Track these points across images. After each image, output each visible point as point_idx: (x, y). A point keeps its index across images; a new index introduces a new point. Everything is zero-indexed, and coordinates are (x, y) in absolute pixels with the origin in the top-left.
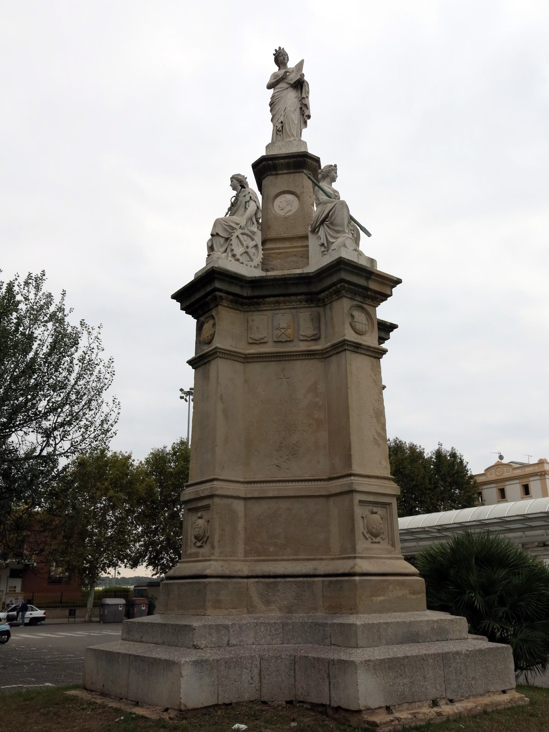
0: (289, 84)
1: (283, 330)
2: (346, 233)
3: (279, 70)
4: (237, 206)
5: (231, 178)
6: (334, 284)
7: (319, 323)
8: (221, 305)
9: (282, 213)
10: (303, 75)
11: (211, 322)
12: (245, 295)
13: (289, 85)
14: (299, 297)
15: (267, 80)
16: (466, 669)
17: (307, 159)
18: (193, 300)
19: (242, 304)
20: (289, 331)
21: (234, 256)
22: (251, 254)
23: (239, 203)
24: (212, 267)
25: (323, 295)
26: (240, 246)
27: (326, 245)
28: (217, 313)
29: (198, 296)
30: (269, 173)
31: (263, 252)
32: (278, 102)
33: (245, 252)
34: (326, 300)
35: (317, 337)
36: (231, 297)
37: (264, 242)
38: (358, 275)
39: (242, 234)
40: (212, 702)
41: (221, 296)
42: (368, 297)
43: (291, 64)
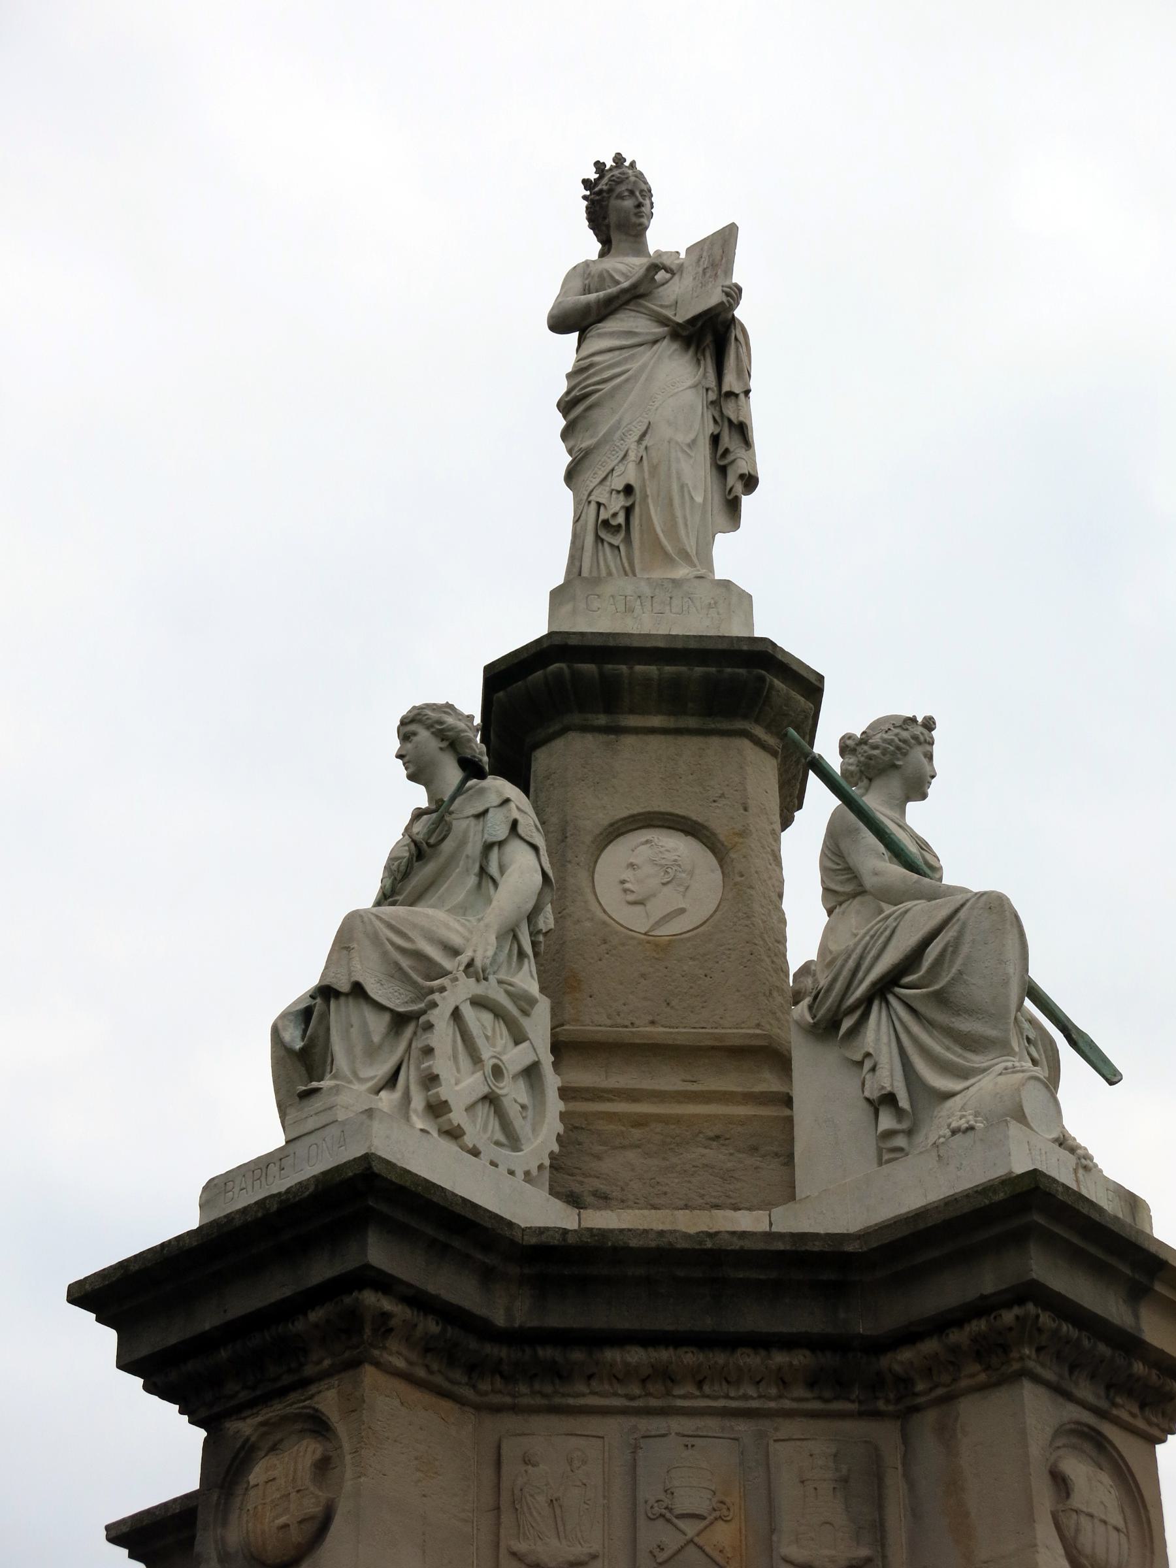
0: (663, 321)
1: (690, 1528)
2: (1010, 1052)
3: (602, 255)
4: (441, 859)
5: (404, 722)
6: (982, 1308)
7: (879, 1503)
8: (377, 1364)
9: (636, 921)
10: (734, 294)
11: (308, 1450)
12: (500, 1319)
13: (656, 326)
14: (780, 1358)
15: (546, 295)
17: (769, 677)
18: (208, 1319)
19: (475, 1368)
20: (723, 1535)
21: (437, 1109)
22: (513, 1111)
23: (448, 846)
24: (367, 1158)
25: (906, 1355)
26: (464, 1061)
27: (904, 1103)
28: (353, 1406)
29: (243, 1302)
30: (576, 718)
31: (561, 1106)
32: (612, 394)
33: (485, 1098)
34: (920, 1387)
36: (432, 1326)
38: (1099, 1270)
39: (478, 1003)
41: (385, 1316)
43: (670, 232)
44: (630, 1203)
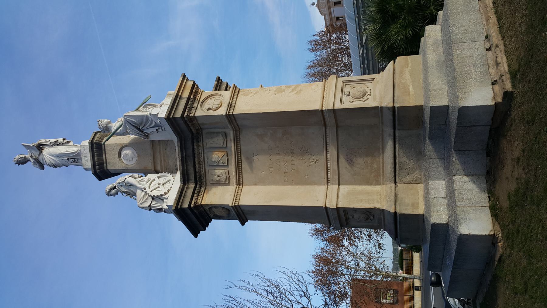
7: (214, 133)
14: (195, 147)
16: (463, 26)
21: (165, 194)
25: (193, 130)
27: (157, 128)
30: (105, 168)
35: (224, 134)
37: (157, 172)
40: (488, 212)
42: (195, 98)
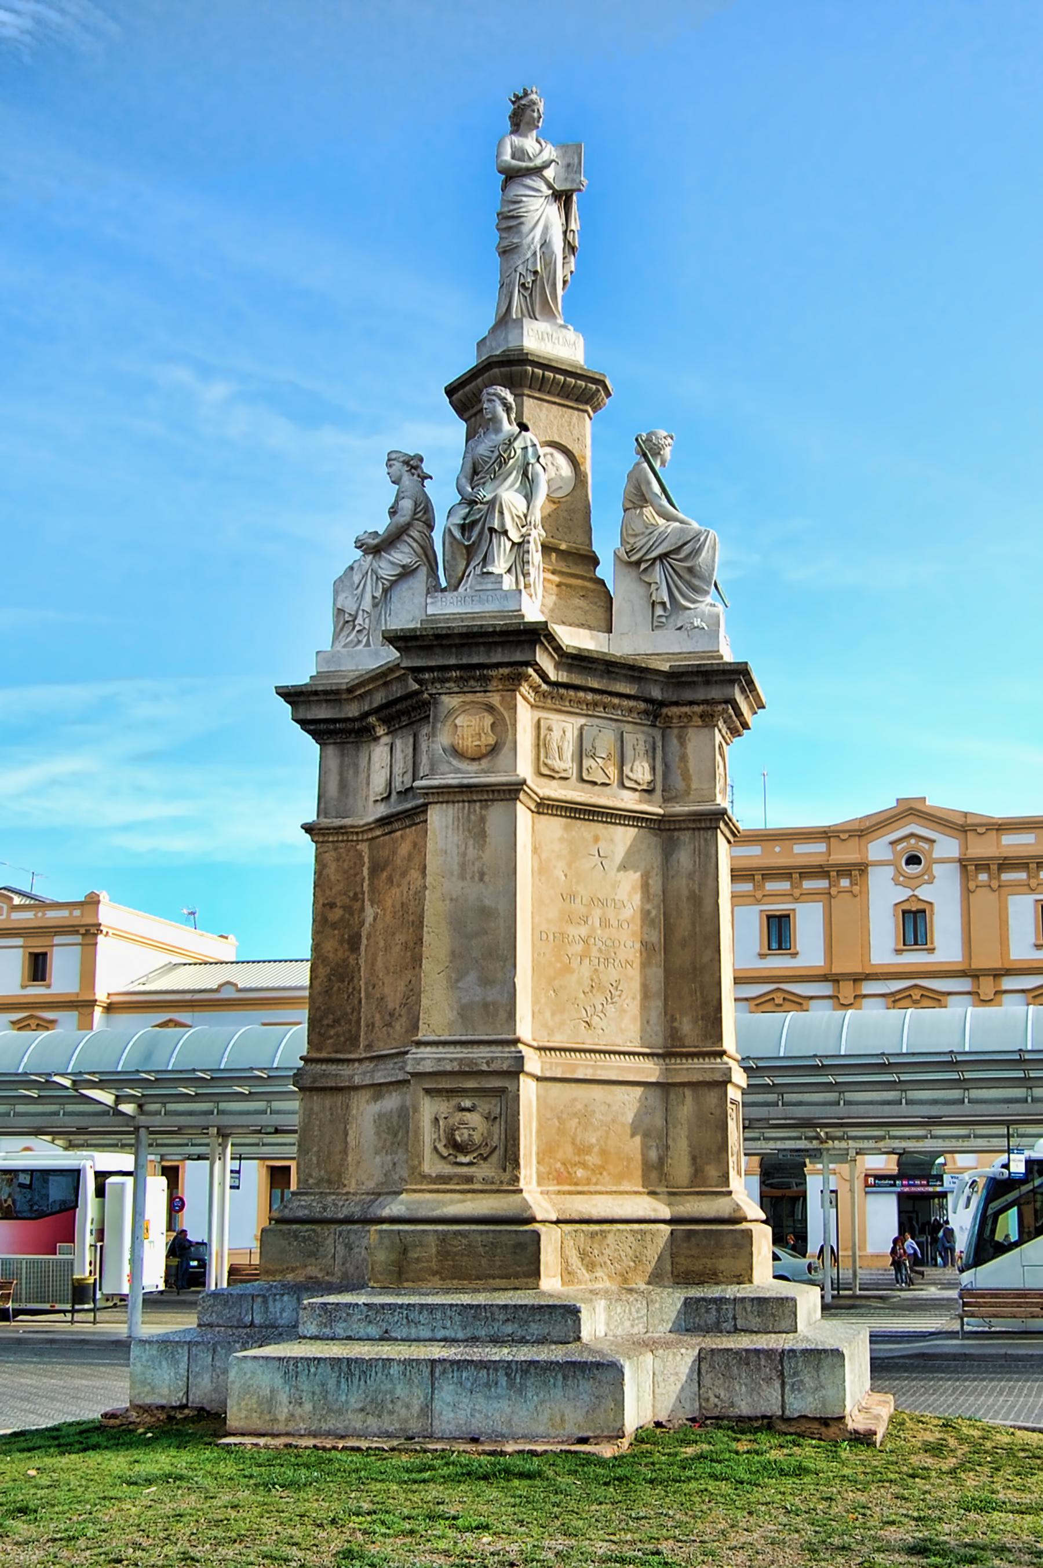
27: (668, 606)
34: (674, 721)
44: (947, 847)
